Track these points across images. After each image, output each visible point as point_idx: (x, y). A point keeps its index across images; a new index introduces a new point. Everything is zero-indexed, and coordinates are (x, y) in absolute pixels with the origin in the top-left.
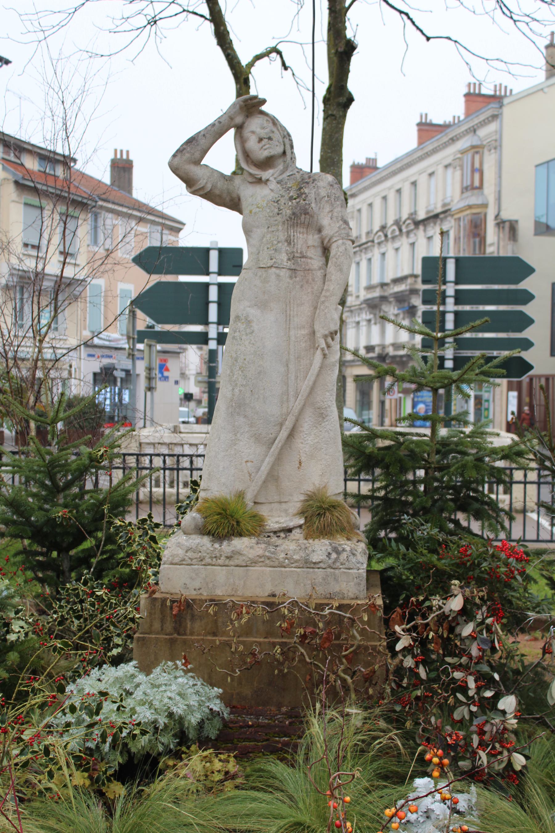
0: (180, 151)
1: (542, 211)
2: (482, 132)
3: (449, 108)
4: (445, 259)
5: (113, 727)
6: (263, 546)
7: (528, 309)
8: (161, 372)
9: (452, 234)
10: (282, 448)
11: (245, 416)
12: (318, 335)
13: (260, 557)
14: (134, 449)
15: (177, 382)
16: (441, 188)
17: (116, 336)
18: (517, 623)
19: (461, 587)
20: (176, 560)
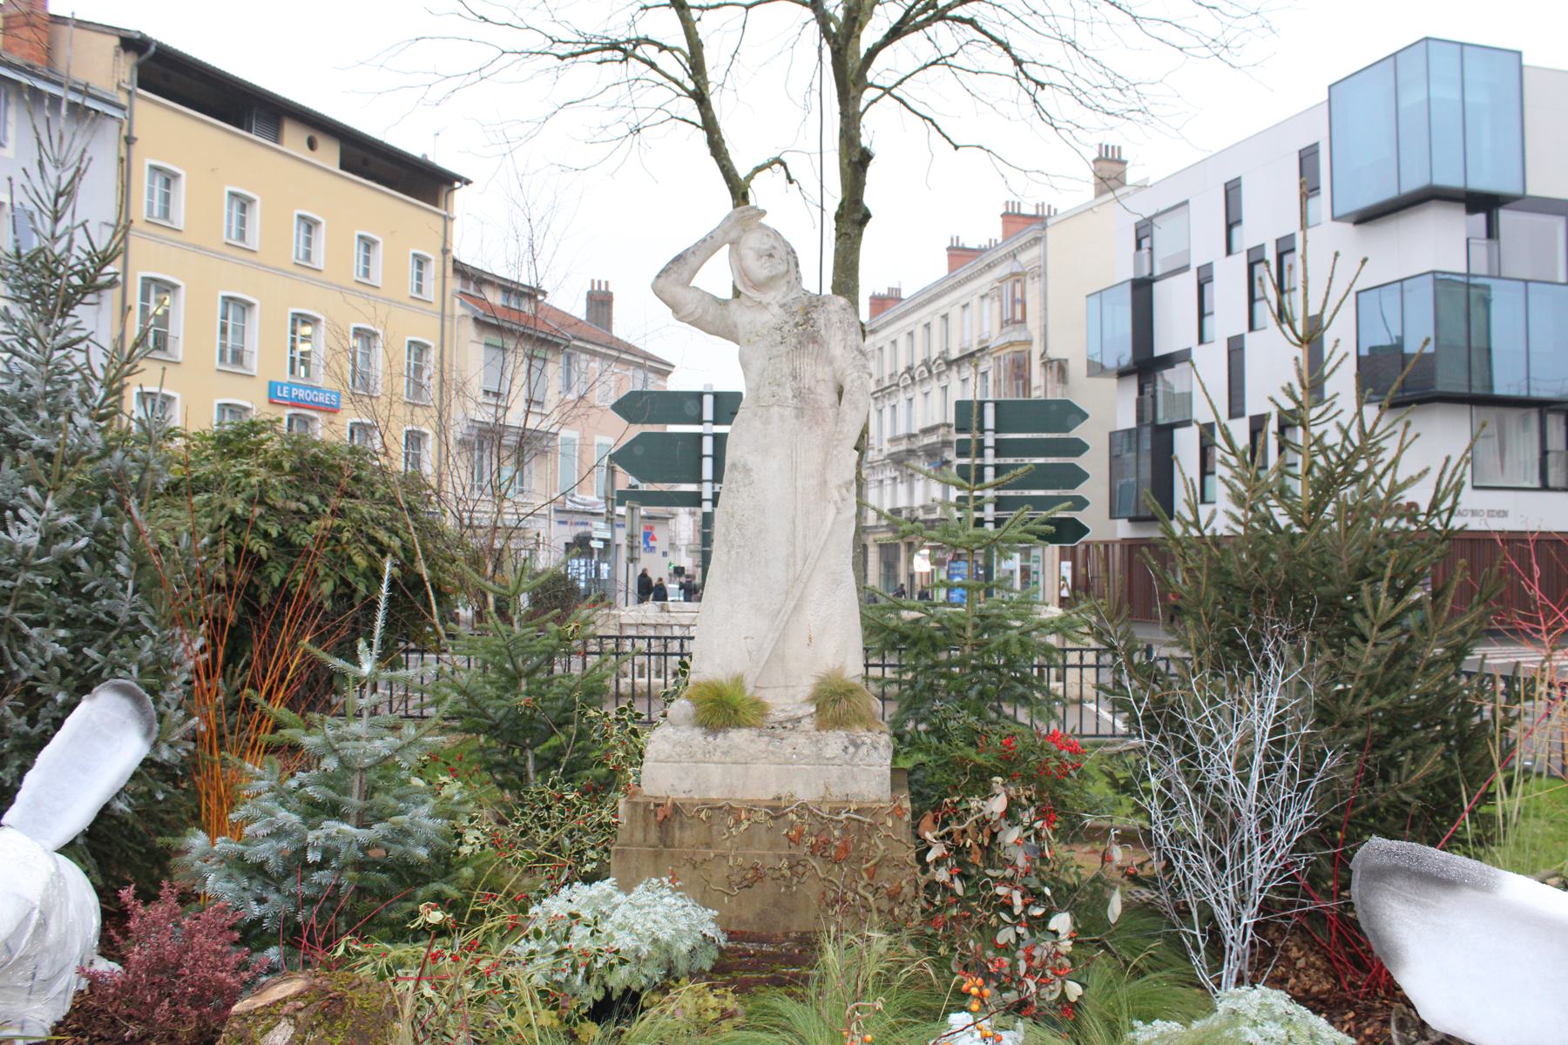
1: (1095, 349)
2: (1024, 258)
3: (984, 230)
4: (982, 404)
5: (586, 955)
6: (767, 739)
7: (1080, 462)
8: (646, 542)
15: (665, 554)
16: (976, 321)
17: (591, 497)
18: (1074, 832)
20: (662, 757)
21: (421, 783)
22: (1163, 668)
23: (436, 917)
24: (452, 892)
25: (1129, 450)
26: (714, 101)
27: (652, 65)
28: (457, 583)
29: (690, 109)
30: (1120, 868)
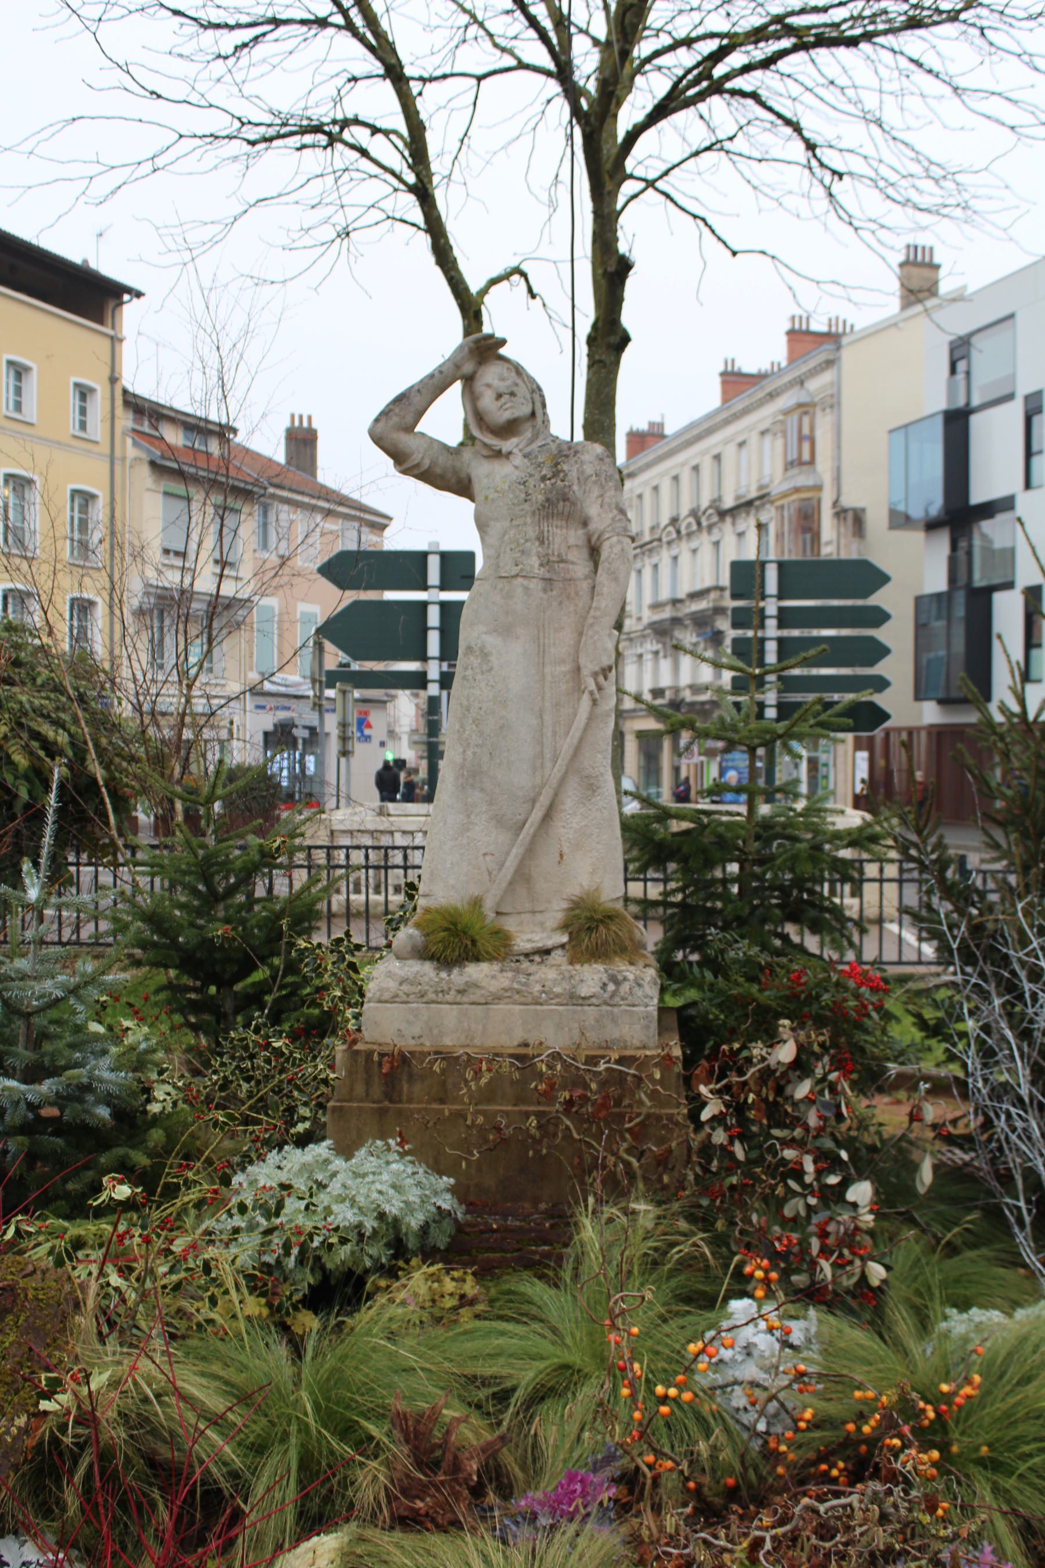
0: (385, 414)
1: (899, 495)
3: (765, 352)
4: (763, 564)
5: (300, 1233)
6: (510, 974)
7: (881, 634)
9: (772, 529)
10: (534, 836)
11: (482, 790)
12: (585, 672)
13: (506, 990)
14: (323, 840)
15: (382, 744)
16: (756, 463)
17: (296, 678)
18: (872, 1080)
19: (793, 1029)
20: (387, 996)
21: (101, 1029)
22: (979, 883)
23: (123, 1192)
24: (141, 1159)
25: (939, 618)
26: (439, 195)
27: (364, 153)
28: (137, 786)
29: (410, 207)
30: (934, 1126)
